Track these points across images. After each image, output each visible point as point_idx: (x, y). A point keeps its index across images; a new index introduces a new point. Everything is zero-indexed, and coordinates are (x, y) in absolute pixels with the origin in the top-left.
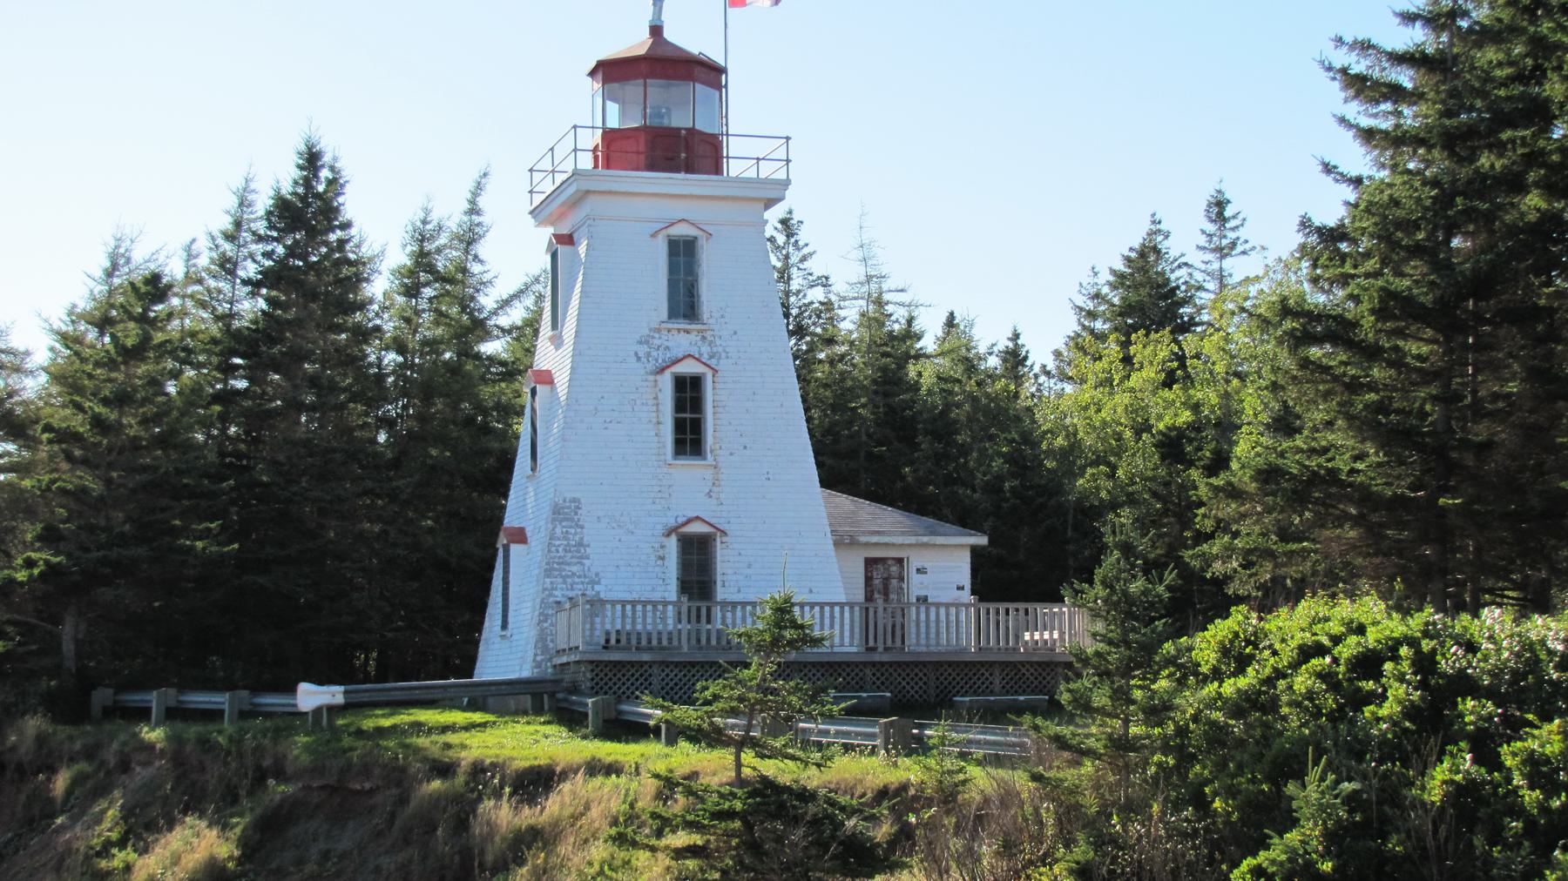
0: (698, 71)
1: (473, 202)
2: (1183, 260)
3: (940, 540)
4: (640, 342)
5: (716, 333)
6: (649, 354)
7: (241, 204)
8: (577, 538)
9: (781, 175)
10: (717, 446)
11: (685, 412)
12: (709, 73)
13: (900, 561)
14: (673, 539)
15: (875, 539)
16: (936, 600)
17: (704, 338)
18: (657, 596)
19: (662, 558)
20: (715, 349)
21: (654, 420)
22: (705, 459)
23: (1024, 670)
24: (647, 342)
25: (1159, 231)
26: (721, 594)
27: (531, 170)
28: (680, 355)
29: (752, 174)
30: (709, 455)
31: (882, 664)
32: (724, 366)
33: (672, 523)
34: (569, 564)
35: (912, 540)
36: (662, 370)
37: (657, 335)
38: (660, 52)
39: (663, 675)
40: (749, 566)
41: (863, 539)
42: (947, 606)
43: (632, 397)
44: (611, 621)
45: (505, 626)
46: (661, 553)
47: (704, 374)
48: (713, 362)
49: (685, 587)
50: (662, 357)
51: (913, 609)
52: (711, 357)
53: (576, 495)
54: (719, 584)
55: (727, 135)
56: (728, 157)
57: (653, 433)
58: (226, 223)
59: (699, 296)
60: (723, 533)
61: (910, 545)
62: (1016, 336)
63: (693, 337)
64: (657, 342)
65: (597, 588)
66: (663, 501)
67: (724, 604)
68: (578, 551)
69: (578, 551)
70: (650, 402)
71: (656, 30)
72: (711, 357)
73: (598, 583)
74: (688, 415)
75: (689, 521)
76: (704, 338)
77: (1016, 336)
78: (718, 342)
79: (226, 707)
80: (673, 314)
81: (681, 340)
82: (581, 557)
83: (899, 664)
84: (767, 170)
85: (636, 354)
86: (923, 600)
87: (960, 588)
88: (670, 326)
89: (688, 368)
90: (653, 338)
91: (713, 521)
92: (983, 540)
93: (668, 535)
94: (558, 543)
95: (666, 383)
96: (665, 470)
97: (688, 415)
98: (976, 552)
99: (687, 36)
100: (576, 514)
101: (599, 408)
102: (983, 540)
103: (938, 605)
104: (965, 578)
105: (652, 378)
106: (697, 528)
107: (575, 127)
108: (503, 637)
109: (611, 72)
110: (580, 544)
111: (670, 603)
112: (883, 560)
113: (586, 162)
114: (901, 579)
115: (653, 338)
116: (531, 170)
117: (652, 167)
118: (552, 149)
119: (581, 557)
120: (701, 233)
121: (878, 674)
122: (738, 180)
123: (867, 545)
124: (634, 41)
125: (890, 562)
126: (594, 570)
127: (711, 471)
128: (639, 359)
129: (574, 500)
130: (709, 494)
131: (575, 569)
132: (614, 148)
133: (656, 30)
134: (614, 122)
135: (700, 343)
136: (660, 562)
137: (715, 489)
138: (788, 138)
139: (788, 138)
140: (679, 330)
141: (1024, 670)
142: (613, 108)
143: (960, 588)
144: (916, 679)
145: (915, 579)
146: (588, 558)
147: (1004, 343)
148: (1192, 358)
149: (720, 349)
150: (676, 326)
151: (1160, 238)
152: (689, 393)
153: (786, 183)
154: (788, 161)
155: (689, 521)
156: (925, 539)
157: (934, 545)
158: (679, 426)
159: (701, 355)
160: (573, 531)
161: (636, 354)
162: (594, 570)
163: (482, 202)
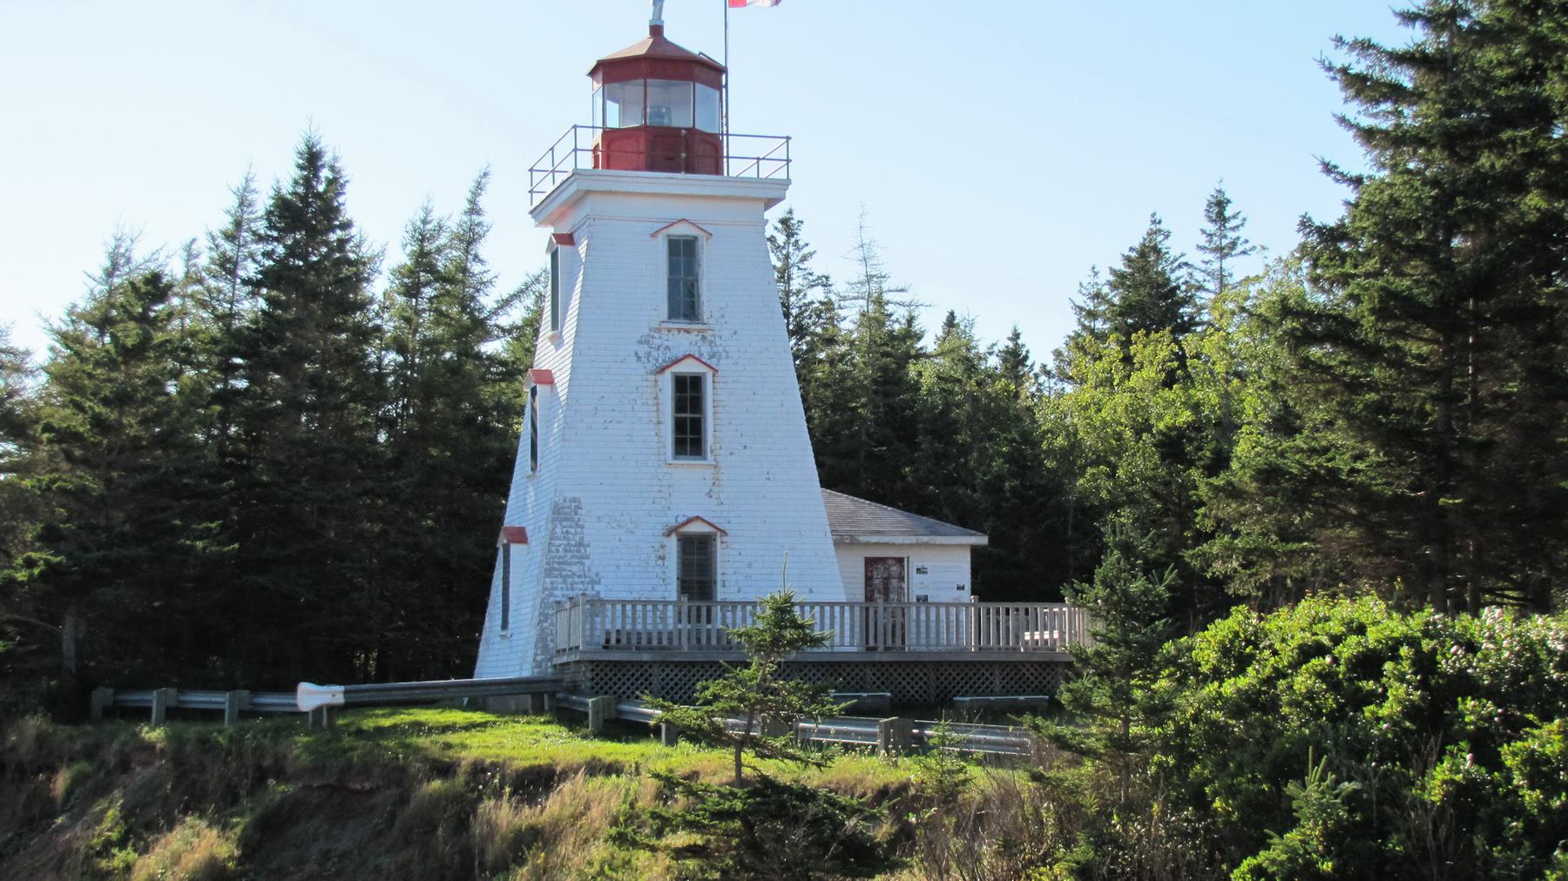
0: (698, 70)
1: (473, 202)
2: (1183, 260)
3: (940, 540)
4: (640, 342)
5: (717, 333)
6: (649, 354)
7: (241, 204)
8: (577, 538)
9: (782, 175)
10: (718, 446)
11: (685, 412)
12: (709, 73)
13: (900, 561)
14: (673, 543)
15: (875, 539)
16: (936, 600)
17: (704, 338)
18: (657, 596)
19: (663, 558)
20: (715, 349)
21: (655, 420)
22: (705, 459)
23: (1024, 670)
24: (647, 342)
25: (1159, 231)
26: (721, 594)
27: (531, 170)
28: (681, 355)
29: (752, 174)
30: (709, 455)
31: (882, 664)
32: (724, 366)
33: (672, 522)
34: (569, 564)
35: (913, 540)
36: (662, 370)
37: (657, 335)
38: (660, 52)
39: (664, 675)
40: (750, 566)
41: (863, 539)
42: (947, 605)
43: (632, 396)
44: (611, 621)
45: (505, 625)
46: (661, 553)
47: (704, 374)
48: (713, 362)
49: (685, 586)
50: (662, 357)
51: (914, 609)
52: (711, 357)
53: (577, 495)
54: (719, 583)
55: (728, 135)
56: (728, 157)
57: (653, 433)
58: (226, 223)
59: (699, 296)
60: (724, 533)
61: (911, 545)
62: (1016, 336)
63: (693, 337)
64: (657, 342)
65: (597, 587)
66: (663, 501)
67: (724, 604)
68: (578, 551)
69: (578, 551)
70: (650, 402)
71: (656, 30)
72: (711, 357)
73: (599, 583)
74: (688, 415)
75: (689, 521)
76: (704, 338)
77: (1016, 336)
78: (718, 342)
79: (226, 707)
80: (673, 313)
81: (681, 340)
82: (581, 557)
83: (899, 664)
84: (767, 170)
85: (636, 354)
86: (923, 600)
87: (961, 588)
88: (670, 326)
89: (688, 368)
90: (653, 337)
91: (713, 521)
92: (983, 540)
93: (669, 535)
94: (558, 542)
95: (667, 384)
96: (665, 470)
97: (688, 415)
98: (976, 551)
99: (687, 36)
100: (576, 513)
101: (600, 408)
102: (983, 540)
103: (938, 605)
104: (966, 578)
105: (652, 378)
106: (697, 528)
107: (575, 127)
108: (503, 637)
109: (611, 71)
110: (580, 544)
111: (670, 602)
112: (883, 560)
113: (586, 161)
114: (901, 579)
115: (653, 337)
116: (531, 170)
117: (652, 167)
118: (552, 149)
119: (581, 557)
120: (701, 233)
121: (878, 674)
122: (739, 180)
123: (867, 544)
124: (635, 41)
125: (890, 562)
126: (594, 570)
127: (712, 471)
128: (639, 359)
129: (575, 500)
130: (709, 495)
131: (575, 568)
132: (614, 148)
133: (656, 30)
134: (614, 122)
135: (700, 343)
136: (660, 562)
137: (715, 489)
138: (788, 138)
139: (788, 138)
140: (679, 330)
141: (1024, 670)
142: (613, 108)
143: (961, 588)
144: (917, 679)
145: (915, 579)
146: (588, 557)
147: (1004, 343)
148: (1193, 357)
149: (720, 349)
150: (677, 326)
151: (1160, 238)
152: (689, 392)
153: (786, 183)
154: (788, 161)
155: (689, 521)
156: (925, 539)
157: (935, 545)
158: (680, 426)
159: (701, 355)
160: (573, 530)
161: (636, 354)
162: (594, 570)
163: (482, 201)
